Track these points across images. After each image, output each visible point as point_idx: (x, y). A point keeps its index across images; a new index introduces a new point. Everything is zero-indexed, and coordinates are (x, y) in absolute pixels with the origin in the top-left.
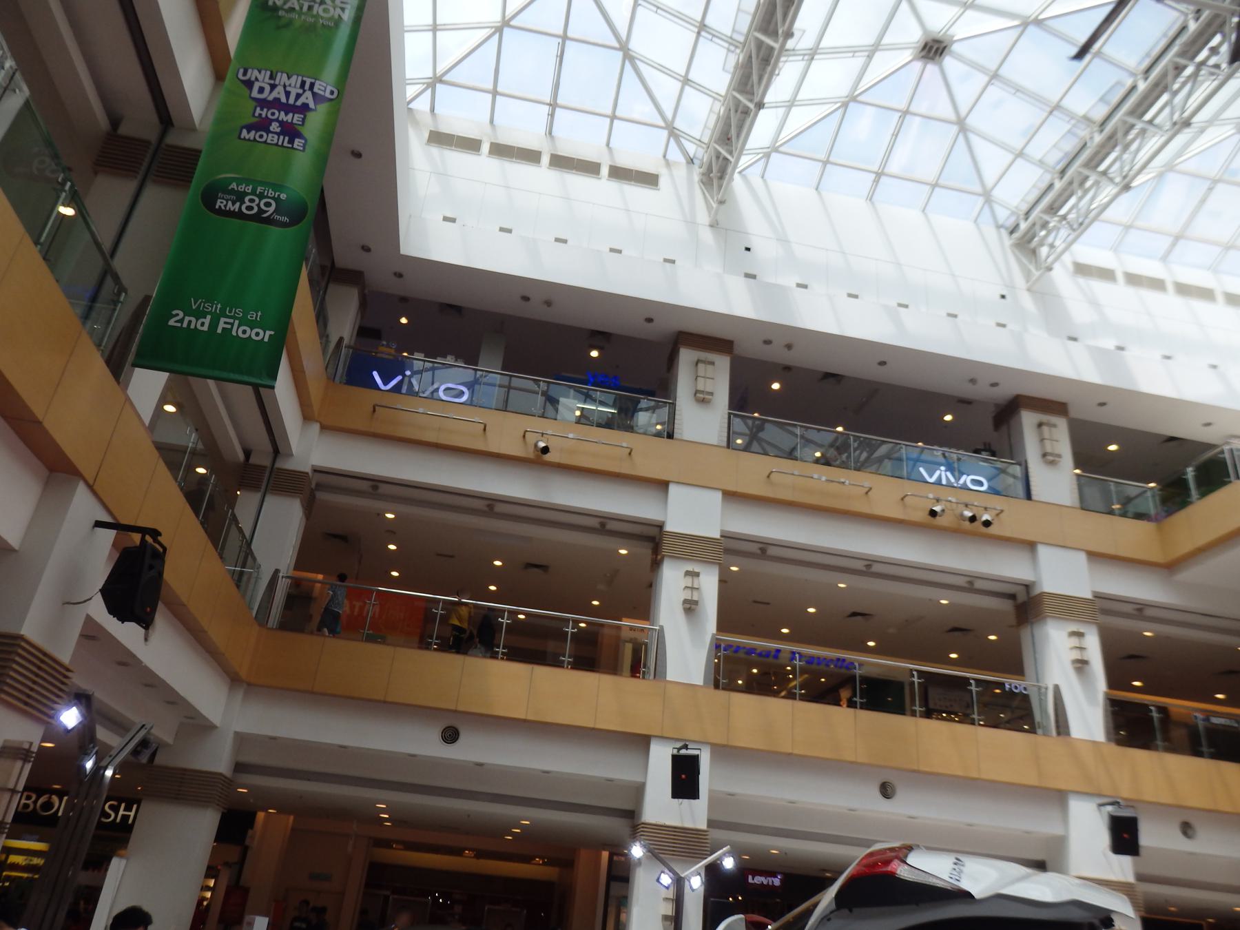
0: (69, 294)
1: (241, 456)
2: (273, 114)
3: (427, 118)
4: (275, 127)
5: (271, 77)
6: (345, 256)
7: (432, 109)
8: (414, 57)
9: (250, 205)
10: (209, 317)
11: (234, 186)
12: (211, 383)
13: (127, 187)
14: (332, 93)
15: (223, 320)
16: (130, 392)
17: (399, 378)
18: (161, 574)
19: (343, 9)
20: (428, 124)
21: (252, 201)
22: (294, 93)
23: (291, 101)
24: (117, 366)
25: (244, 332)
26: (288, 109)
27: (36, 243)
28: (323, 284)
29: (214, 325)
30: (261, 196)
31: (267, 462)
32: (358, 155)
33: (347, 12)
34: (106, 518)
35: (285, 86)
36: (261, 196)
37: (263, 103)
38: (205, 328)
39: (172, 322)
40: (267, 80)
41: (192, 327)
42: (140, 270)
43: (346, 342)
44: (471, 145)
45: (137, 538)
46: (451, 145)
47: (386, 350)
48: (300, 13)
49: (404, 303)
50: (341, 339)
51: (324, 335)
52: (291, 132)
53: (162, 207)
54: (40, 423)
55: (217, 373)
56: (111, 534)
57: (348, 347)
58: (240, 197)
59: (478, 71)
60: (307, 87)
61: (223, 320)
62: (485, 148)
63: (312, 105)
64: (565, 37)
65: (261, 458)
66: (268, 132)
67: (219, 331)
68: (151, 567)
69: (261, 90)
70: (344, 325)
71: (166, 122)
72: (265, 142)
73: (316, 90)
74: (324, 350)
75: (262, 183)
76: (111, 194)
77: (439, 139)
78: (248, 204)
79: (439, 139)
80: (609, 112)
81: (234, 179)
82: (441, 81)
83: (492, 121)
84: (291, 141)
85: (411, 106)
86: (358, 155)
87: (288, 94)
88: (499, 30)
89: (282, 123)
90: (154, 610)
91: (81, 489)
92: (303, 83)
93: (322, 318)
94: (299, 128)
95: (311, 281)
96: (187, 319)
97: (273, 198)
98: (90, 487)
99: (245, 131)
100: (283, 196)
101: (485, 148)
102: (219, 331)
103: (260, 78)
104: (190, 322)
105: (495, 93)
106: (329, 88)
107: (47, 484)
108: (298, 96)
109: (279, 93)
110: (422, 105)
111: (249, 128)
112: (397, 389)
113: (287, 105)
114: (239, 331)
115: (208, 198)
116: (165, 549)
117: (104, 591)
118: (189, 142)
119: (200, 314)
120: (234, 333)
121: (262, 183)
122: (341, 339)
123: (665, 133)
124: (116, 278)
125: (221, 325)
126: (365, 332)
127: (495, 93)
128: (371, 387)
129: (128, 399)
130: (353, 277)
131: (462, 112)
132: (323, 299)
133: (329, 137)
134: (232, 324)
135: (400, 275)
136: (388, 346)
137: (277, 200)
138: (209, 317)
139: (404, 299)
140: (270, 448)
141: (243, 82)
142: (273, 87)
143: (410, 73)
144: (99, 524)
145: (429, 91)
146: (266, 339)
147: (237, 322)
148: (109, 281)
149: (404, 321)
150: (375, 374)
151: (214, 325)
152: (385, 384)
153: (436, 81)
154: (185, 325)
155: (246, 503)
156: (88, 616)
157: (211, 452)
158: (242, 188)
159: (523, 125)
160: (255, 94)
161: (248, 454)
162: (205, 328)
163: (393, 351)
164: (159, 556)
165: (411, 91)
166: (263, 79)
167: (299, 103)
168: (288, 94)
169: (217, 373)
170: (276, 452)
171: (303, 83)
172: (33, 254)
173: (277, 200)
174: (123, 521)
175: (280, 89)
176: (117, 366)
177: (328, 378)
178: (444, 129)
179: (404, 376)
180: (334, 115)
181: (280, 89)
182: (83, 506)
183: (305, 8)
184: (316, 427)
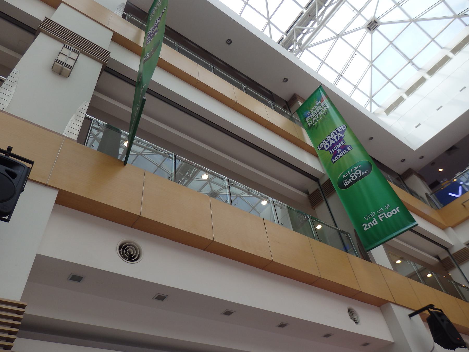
0: (341, 250)
1: (436, 260)
2: (335, 148)
3: (380, 109)
4: (339, 151)
5: (326, 141)
6: (400, 169)
7: (379, 106)
8: (359, 100)
9: (353, 177)
10: (374, 219)
11: (344, 176)
12: (394, 239)
13: (323, 206)
14: (344, 127)
15: (379, 216)
16: (377, 263)
17: (460, 188)
18: (449, 321)
19: (326, 106)
20: (382, 110)
21: (353, 175)
22: (335, 138)
23: (336, 140)
24: (366, 257)
25: (389, 214)
26: (337, 143)
27: (314, 239)
28: (403, 183)
29: (378, 219)
30: (354, 172)
31: (447, 255)
32: (372, 138)
33: (327, 105)
34: (411, 312)
35: (331, 139)
36: (354, 172)
37: (330, 149)
38: (377, 223)
39: (365, 229)
40: (326, 142)
41: (372, 226)
42: (346, 224)
43: (429, 193)
44: (400, 100)
45: (427, 312)
46: (394, 107)
47: (445, 184)
48: (318, 119)
49: (434, 164)
50: (426, 194)
51: (420, 198)
52: (344, 148)
53: (335, 201)
54: (361, 292)
55: (395, 234)
56: (417, 317)
57: (431, 194)
58: (349, 177)
59: (379, 80)
60: (336, 133)
61: (379, 216)
62: (405, 96)
63: (342, 136)
64: (391, 43)
65: (444, 255)
66: (339, 154)
67: (382, 220)
68: (443, 320)
69: (327, 146)
70: (423, 189)
71: (316, 180)
72: (341, 157)
73: (339, 131)
74: (428, 204)
75: (351, 168)
76: (322, 210)
77: (389, 110)
78: (352, 177)
79: (389, 110)
80: (430, 40)
81: (343, 174)
82: (373, 97)
83: (398, 88)
84: (347, 150)
85: (372, 112)
86: (372, 138)
87: (334, 140)
88: (372, 65)
89: (339, 148)
90: (461, 339)
91: (394, 307)
92: (335, 133)
93: (412, 193)
94: (345, 144)
95: (395, 184)
96: (369, 224)
97: (358, 169)
98: (395, 304)
99: (333, 160)
100: (360, 166)
101: (405, 96)
102: (382, 220)
103: (324, 144)
104: (370, 225)
105: (390, 81)
106: (342, 127)
107: (383, 312)
108: (337, 137)
109: (332, 142)
110: (375, 108)
111: (333, 158)
112: (464, 191)
113: (336, 142)
114: (387, 215)
115: (342, 186)
116: (441, 310)
117: (436, 340)
118: (325, 179)
119: (371, 220)
120: (387, 217)
121: (351, 168)
122: (426, 194)
123: (457, 20)
124: (343, 232)
125: (381, 218)
126: (433, 186)
127: (390, 81)
128: (455, 199)
129: (379, 265)
130: (409, 172)
131: (387, 96)
132: (407, 187)
133: (356, 139)
134: (383, 215)
135: (422, 157)
136: (444, 182)
137: (359, 168)
138: (374, 219)
139: (433, 163)
140: (443, 250)
141: (321, 149)
142: (329, 142)
143: (363, 105)
144: (411, 316)
145: (372, 103)
146: (399, 211)
147: (384, 213)
148: (342, 234)
149: (441, 170)
150: (450, 194)
151: (378, 219)
152: (458, 194)
153: (371, 99)
154: (370, 227)
155: (455, 274)
156: (15, 339)
157: (427, 267)
158: (347, 174)
159: (409, 76)
160: (326, 149)
161: (437, 257)
162: (377, 223)
163: (448, 182)
164: (441, 314)
165: (368, 108)
166: (325, 143)
167: (339, 139)
168: (334, 140)
169: (395, 234)
170: (446, 249)
171: (335, 133)
172: (316, 242)
173: (359, 168)
174: (417, 309)
175: (331, 141)
176: (366, 257)
177: (436, 210)
178: (387, 106)
179: (461, 185)
180: (351, 131)
181: (331, 141)
182: (400, 313)
183: (318, 117)
184: (450, 229)
